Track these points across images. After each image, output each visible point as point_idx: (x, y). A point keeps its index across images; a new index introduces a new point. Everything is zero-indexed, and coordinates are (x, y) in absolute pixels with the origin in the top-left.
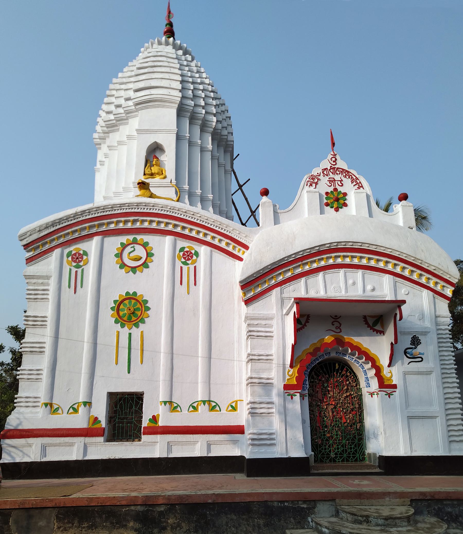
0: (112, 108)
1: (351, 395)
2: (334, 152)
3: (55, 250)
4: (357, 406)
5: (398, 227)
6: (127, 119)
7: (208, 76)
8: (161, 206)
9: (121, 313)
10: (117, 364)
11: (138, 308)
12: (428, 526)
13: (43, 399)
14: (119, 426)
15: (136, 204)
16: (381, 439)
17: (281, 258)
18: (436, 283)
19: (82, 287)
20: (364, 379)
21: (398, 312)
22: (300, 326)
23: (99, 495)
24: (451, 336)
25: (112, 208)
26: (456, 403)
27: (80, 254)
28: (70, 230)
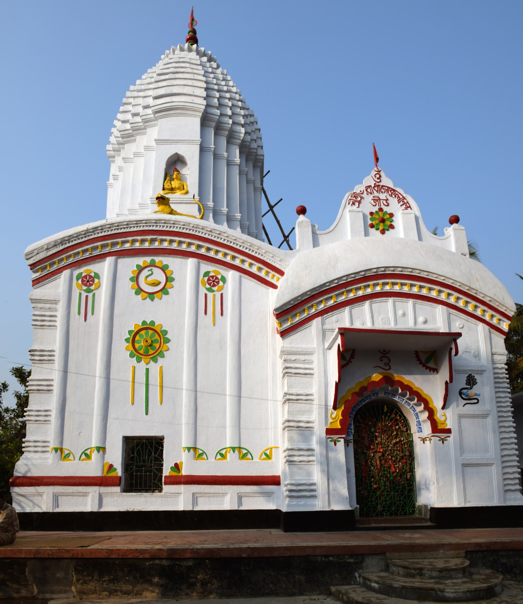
0: (129, 116)
1: (400, 441)
2: (377, 168)
3: (64, 272)
4: (407, 453)
5: (450, 252)
6: (145, 129)
7: (238, 91)
8: (183, 224)
9: (137, 346)
12: (483, 577)
13: (53, 444)
14: (136, 476)
15: (154, 221)
16: (433, 488)
17: (322, 283)
18: (492, 316)
20: (415, 423)
21: (453, 346)
22: (345, 362)
23: (119, 547)
24: (507, 376)
25: (127, 225)
26: (512, 449)
27: (91, 277)
28: (80, 249)
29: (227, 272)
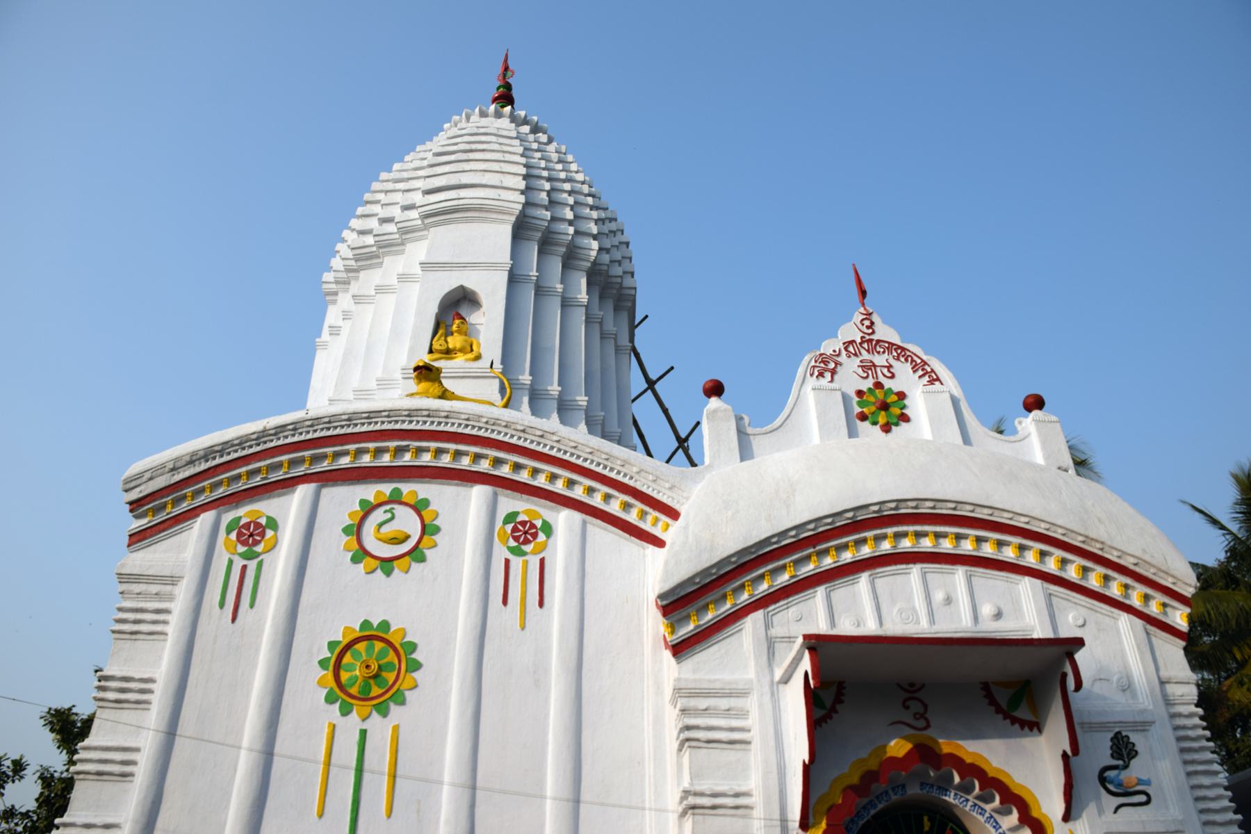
0: (373, 224)
6: (402, 244)
9: (344, 676)
10: (321, 815)
11: (391, 664)
17: (763, 536)
19: (252, 606)
21: (1068, 669)
25: (349, 420)
27: (258, 525)
29: (555, 514)
